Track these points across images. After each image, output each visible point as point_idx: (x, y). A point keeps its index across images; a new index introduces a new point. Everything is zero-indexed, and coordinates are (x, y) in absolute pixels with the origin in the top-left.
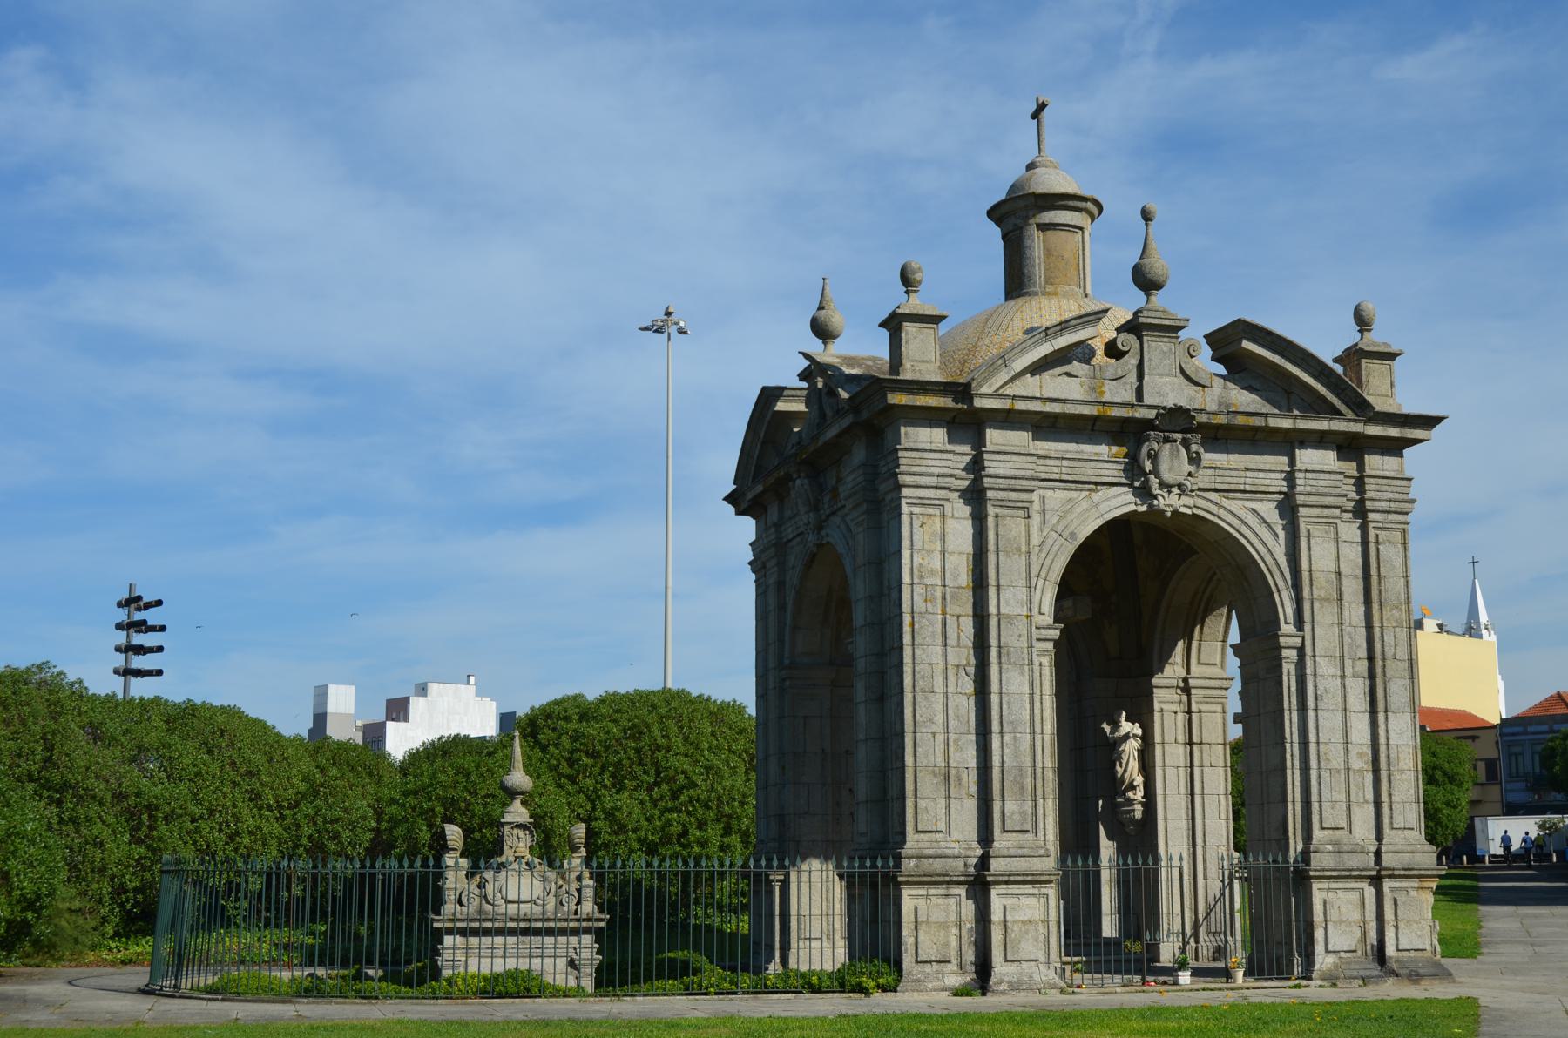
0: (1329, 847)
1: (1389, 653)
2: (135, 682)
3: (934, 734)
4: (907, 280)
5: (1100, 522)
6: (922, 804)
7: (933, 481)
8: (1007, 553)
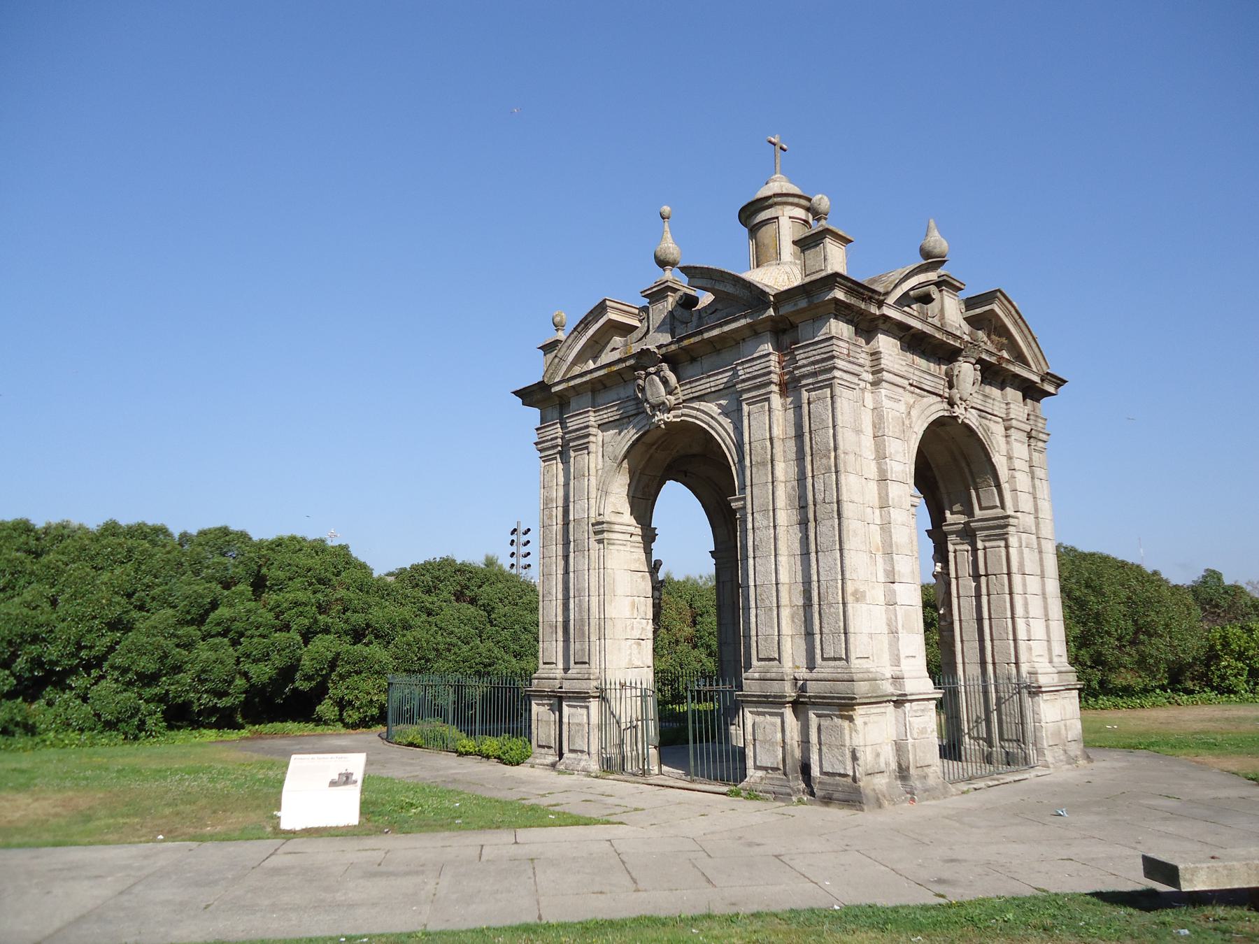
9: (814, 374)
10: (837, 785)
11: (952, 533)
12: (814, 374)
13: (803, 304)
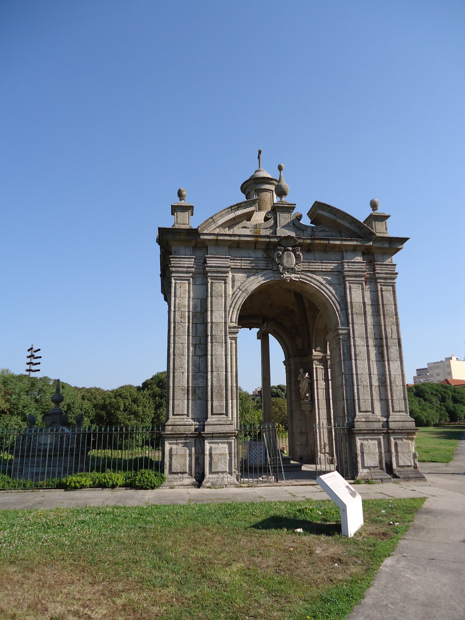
0: (363, 420)
1: (389, 335)
2: (31, 373)
3: (183, 373)
4: (180, 194)
5: (258, 285)
6: (176, 402)
7: (185, 269)
8: (216, 297)
9: (385, 279)
10: (408, 471)
11: (315, 360)
12: (385, 279)
13: (386, 245)
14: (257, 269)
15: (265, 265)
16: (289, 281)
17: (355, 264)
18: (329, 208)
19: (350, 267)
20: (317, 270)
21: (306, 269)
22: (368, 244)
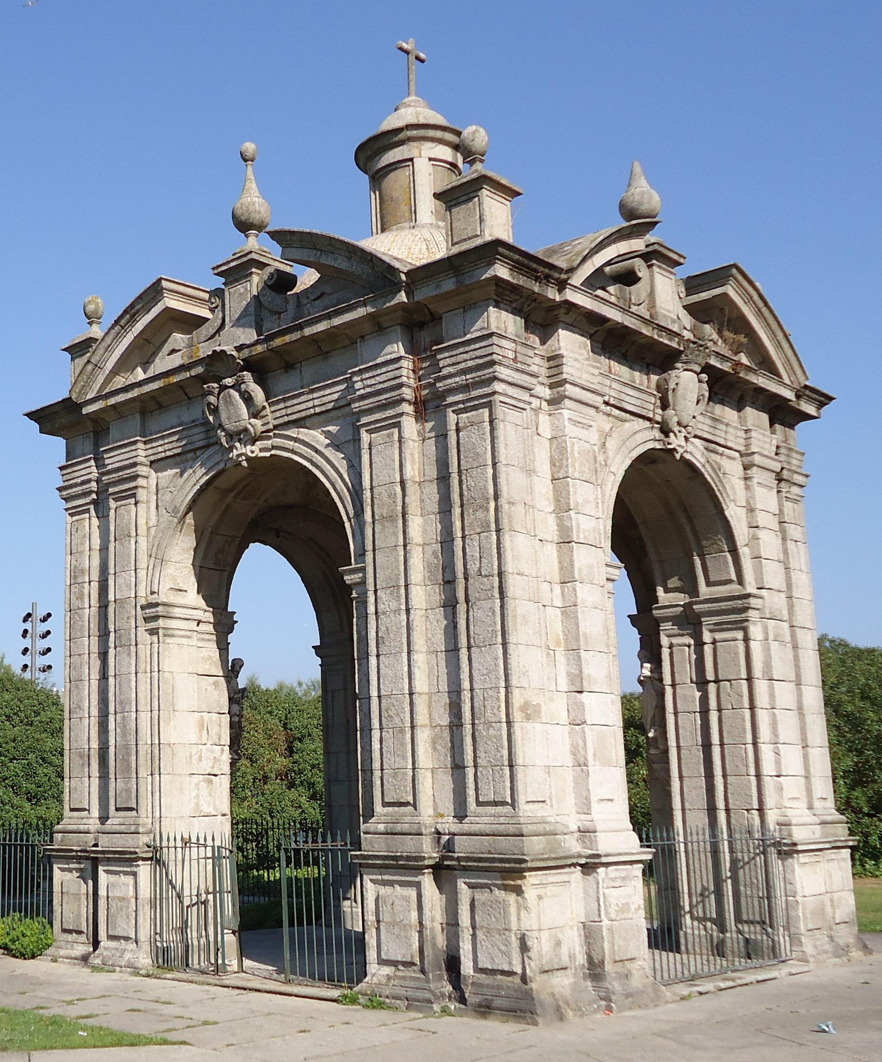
9: (465, 388)
10: (499, 987)
11: (666, 619)
12: (465, 388)
14: (194, 450)
15: (203, 436)
16: (245, 464)
17: (379, 372)
18: (295, 238)
19: (369, 382)
20: (303, 414)
21: (281, 421)
22: (392, 303)
